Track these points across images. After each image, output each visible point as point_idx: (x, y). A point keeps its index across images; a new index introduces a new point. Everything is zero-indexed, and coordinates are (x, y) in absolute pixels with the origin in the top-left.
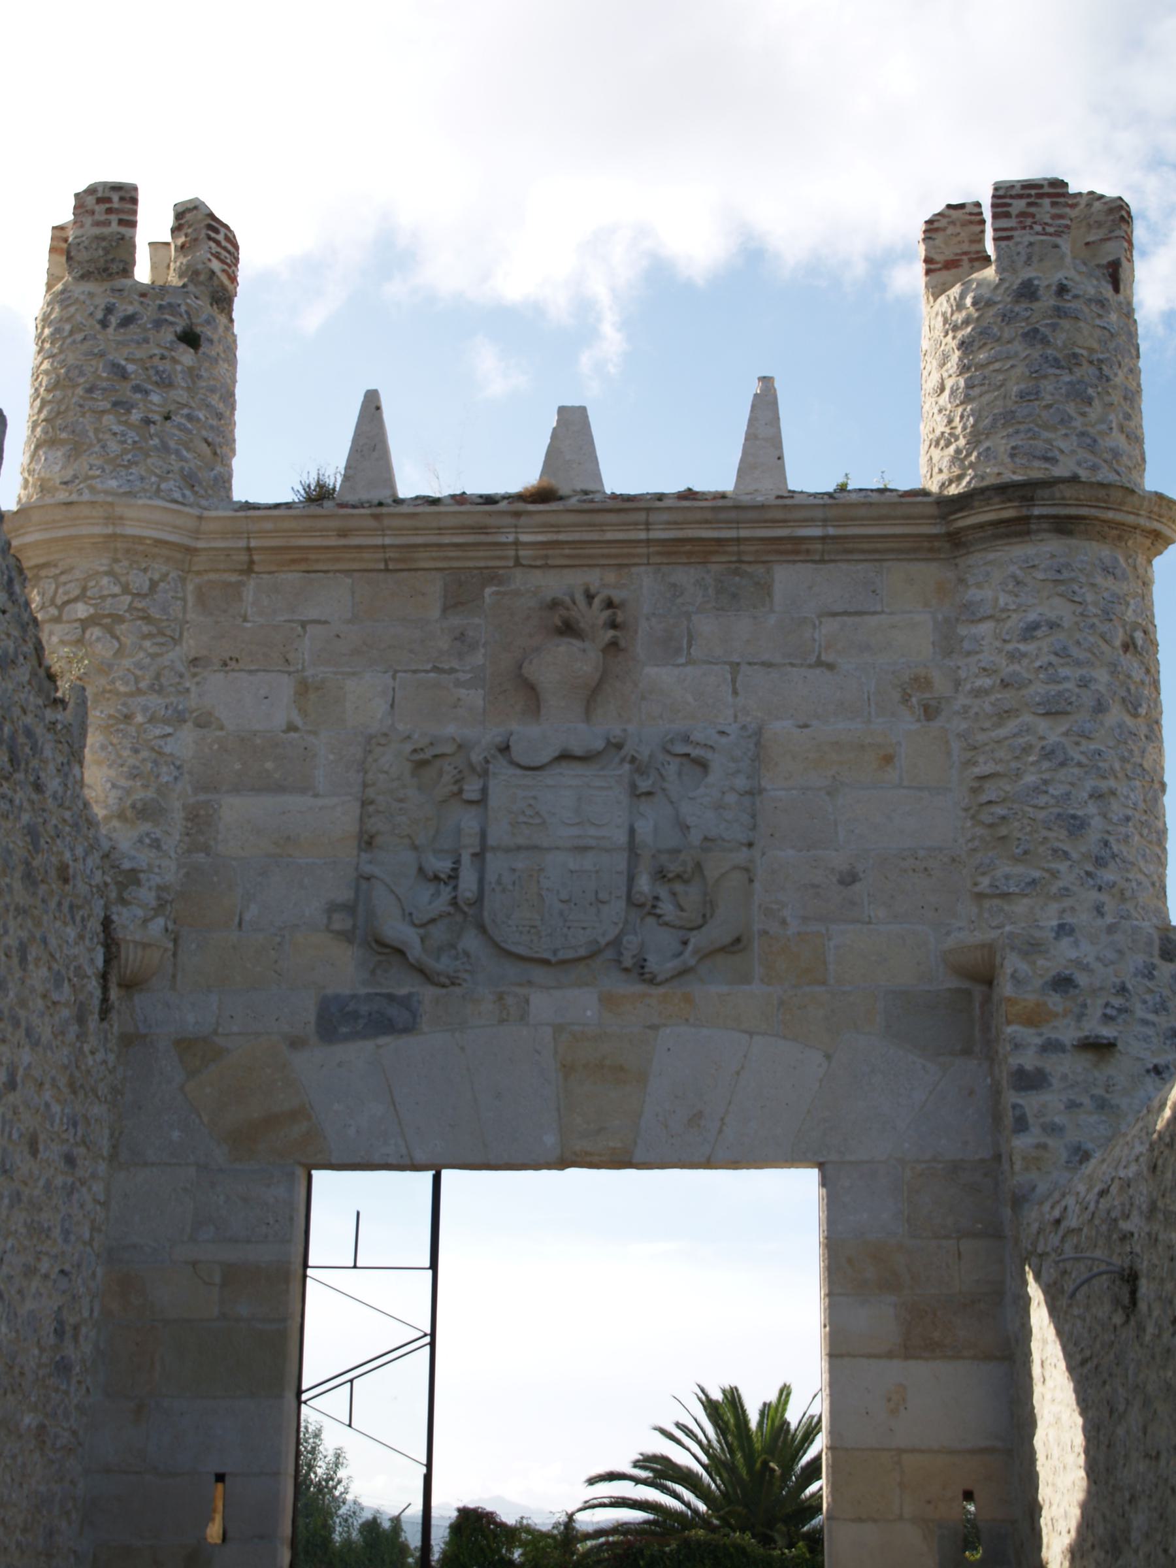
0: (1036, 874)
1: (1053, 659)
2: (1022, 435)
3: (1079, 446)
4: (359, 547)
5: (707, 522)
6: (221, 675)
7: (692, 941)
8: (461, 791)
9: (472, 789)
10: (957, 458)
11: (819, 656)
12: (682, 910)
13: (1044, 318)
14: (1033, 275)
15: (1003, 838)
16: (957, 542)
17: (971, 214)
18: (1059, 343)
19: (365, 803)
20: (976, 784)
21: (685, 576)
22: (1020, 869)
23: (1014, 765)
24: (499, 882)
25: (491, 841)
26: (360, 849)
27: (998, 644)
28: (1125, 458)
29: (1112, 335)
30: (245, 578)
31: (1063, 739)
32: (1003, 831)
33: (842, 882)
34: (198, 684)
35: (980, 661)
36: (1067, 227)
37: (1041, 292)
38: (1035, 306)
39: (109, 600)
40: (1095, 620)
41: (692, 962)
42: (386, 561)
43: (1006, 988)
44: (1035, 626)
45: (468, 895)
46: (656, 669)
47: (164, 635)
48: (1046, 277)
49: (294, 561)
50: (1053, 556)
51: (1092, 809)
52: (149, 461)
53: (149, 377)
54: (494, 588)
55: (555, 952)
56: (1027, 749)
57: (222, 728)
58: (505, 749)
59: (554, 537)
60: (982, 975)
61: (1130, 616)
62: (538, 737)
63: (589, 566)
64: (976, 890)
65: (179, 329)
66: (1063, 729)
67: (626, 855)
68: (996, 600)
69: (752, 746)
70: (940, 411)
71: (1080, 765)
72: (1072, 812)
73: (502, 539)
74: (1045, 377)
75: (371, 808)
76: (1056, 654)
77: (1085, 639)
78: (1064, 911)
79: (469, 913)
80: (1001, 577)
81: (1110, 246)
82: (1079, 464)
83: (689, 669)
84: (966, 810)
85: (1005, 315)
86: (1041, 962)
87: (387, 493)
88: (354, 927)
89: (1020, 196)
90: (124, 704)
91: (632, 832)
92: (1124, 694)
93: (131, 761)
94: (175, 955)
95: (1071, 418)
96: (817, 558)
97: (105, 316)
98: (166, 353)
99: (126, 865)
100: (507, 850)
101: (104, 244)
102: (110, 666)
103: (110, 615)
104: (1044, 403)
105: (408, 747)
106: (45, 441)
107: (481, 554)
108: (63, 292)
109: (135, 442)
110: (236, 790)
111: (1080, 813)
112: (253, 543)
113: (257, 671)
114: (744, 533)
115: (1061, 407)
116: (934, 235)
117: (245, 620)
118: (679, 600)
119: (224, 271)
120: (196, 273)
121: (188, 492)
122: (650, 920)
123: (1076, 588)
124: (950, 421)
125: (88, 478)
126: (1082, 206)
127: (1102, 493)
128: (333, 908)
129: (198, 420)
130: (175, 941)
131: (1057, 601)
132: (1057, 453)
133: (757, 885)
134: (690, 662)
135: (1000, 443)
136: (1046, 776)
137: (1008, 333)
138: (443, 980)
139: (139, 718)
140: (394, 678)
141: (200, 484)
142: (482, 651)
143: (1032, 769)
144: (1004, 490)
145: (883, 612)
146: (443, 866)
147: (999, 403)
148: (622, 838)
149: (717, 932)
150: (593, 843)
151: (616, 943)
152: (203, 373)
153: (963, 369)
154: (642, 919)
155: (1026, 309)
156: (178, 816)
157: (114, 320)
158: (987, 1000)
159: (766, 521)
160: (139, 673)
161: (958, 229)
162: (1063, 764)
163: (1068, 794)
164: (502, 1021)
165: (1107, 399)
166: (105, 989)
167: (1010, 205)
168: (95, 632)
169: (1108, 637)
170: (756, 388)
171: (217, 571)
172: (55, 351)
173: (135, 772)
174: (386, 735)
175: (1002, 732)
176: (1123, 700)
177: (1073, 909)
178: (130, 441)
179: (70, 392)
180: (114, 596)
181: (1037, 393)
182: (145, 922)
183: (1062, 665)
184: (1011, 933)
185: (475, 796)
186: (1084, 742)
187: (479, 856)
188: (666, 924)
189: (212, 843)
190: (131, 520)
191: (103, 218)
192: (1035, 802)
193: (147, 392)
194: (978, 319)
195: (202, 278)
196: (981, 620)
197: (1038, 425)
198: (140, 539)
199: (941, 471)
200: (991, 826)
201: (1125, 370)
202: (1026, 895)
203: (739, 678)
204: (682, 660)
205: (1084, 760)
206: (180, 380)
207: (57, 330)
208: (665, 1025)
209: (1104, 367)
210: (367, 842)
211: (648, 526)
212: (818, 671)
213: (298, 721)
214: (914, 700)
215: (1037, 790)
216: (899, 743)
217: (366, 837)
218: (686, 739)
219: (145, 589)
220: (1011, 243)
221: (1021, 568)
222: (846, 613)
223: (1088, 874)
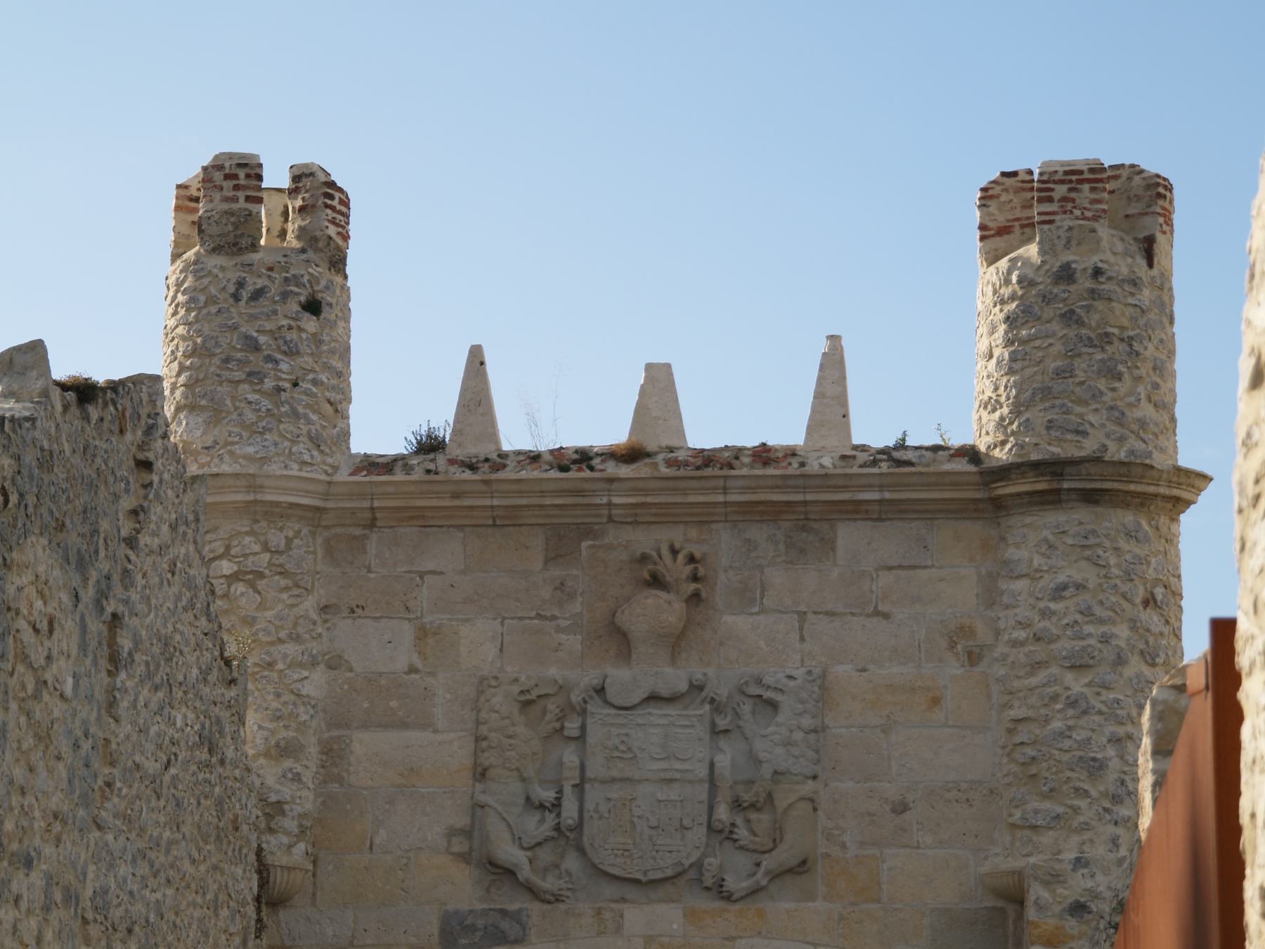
0: (1061, 810)
1: (1078, 617)
2: (1057, 410)
3: (1108, 419)
4: (471, 507)
5: (777, 487)
6: (349, 621)
7: (764, 863)
8: (562, 728)
9: (572, 727)
10: (1001, 424)
11: (876, 607)
12: (755, 835)
13: (1080, 300)
14: (1071, 258)
15: (1033, 776)
16: (999, 506)
17: (1023, 182)
18: (1093, 324)
19: (478, 739)
20: (1011, 726)
21: (758, 533)
22: (1047, 805)
23: (1043, 711)
24: (596, 810)
25: (589, 774)
26: (475, 780)
27: (1031, 601)
28: (1151, 426)
29: (1143, 311)
30: (367, 532)
31: (1085, 690)
32: (1033, 770)
33: (894, 811)
34: (328, 629)
35: (1016, 615)
36: (1104, 211)
37: (1078, 275)
38: (1072, 288)
39: (251, 558)
40: (1118, 582)
41: (764, 882)
42: (494, 519)
43: (1031, 913)
44: (1064, 587)
45: (570, 822)
46: (733, 617)
47: (298, 586)
48: (1083, 261)
49: (411, 518)
50: (1081, 523)
51: (1111, 752)
52: (282, 426)
53: (279, 347)
54: (590, 543)
55: (645, 873)
56: (1055, 698)
57: (351, 670)
58: (601, 691)
59: (643, 499)
60: (1012, 896)
61: (1151, 574)
62: (626, 679)
63: (674, 522)
64: (1010, 820)
65: (303, 299)
66: (1086, 681)
67: (706, 786)
68: (1031, 560)
69: (816, 689)
70: (988, 377)
71: (1100, 713)
72: (1093, 755)
73: (598, 501)
74: (1079, 355)
75: (484, 744)
76: (1081, 613)
77: (1107, 599)
78: (1083, 843)
79: (569, 837)
80: (1032, 537)
81: (1147, 220)
82: (1108, 436)
83: (761, 618)
84: (1003, 748)
85: (1044, 297)
86: (1060, 891)
87: (493, 447)
88: (471, 849)
89: (1062, 182)
90: (266, 653)
91: (712, 765)
92: (1142, 646)
93: (275, 705)
94: (314, 875)
95: (1101, 393)
96: (875, 516)
97: (237, 290)
98: (293, 323)
99: (273, 798)
100: (603, 782)
101: (232, 219)
102: (254, 619)
103: (252, 572)
104: (1078, 380)
105: (516, 689)
106: (185, 406)
107: (578, 512)
108: (195, 263)
109: (268, 410)
110: (365, 726)
111: (1099, 756)
112: (376, 504)
113: (381, 617)
114: (809, 497)
115: (1092, 383)
116: (989, 203)
117: (369, 571)
118: (753, 554)
119: (339, 233)
120: (315, 239)
121: (315, 453)
122: (727, 844)
123: (1100, 552)
124: (996, 389)
125: (227, 444)
126: (1123, 179)
127: (1124, 470)
128: (452, 833)
129: (322, 383)
130: (315, 863)
131: (1084, 564)
132: (1088, 426)
133: (820, 813)
134: (763, 611)
135: (1038, 415)
136: (1071, 723)
137: (1048, 312)
138: (548, 897)
139: (280, 666)
140: (502, 624)
141: (325, 443)
142: (580, 599)
143: (1058, 716)
144: (1037, 467)
145: (933, 566)
146: (548, 795)
147: (1039, 378)
148: (703, 772)
149: (784, 856)
150: (678, 775)
151: (698, 865)
152: (326, 338)
153: (1009, 342)
154: (721, 843)
155: (1064, 291)
156: (313, 750)
157: (245, 295)
158: (1020, 916)
159: (829, 487)
160: (278, 623)
161: (1011, 196)
162: (1085, 712)
163: (1089, 739)
164: (600, 933)
165: (1136, 372)
166: (259, 910)
167: (1052, 190)
168: (240, 588)
169: (1129, 596)
170: (823, 346)
171: (343, 525)
172: (191, 319)
173: (278, 714)
174: (496, 678)
175: (1033, 681)
176: (1142, 652)
177: (1091, 841)
178: (264, 409)
179: (207, 361)
180: (256, 554)
181: (1071, 371)
182: (290, 846)
183: (1087, 623)
184: (1035, 865)
185: (576, 733)
186: (1104, 692)
187: (579, 787)
188: (741, 848)
189: (345, 774)
190: (270, 488)
191: (231, 194)
192: (1060, 745)
193: (276, 362)
194: (1022, 296)
195: (321, 245)
196: (1018, 577)
197: (1072, 401)
198: (278, 504)
199: (988, 433)
200: (1024, 764)
201: (1155, 341)
202: (1051, 828)
203: (806, 626)
204: (756, 609)
205: (1104, 709)
206: (303, 348)
207: (192, 300)
208: (741, 937)
209: (1134, 343)
210: (481, 774)
211: (725, 490)
212: (875, 620)
213: (418, 663)
214: (959, 647)
215: (1063, 735)
216: (946, 687)
217: (480, 769)
218: (759, 682)
219: (282, 547)
220: (1052, 227)
221: (1053, 534)
222: (900, 567)
223: (1106, 810)
